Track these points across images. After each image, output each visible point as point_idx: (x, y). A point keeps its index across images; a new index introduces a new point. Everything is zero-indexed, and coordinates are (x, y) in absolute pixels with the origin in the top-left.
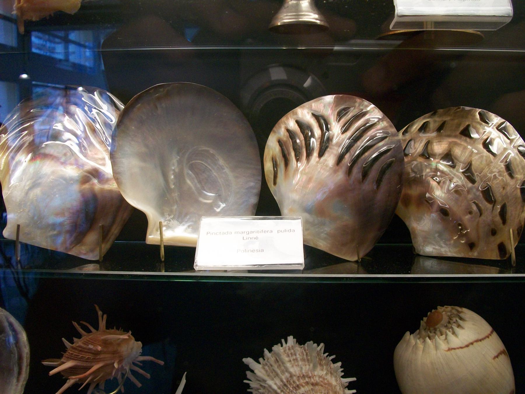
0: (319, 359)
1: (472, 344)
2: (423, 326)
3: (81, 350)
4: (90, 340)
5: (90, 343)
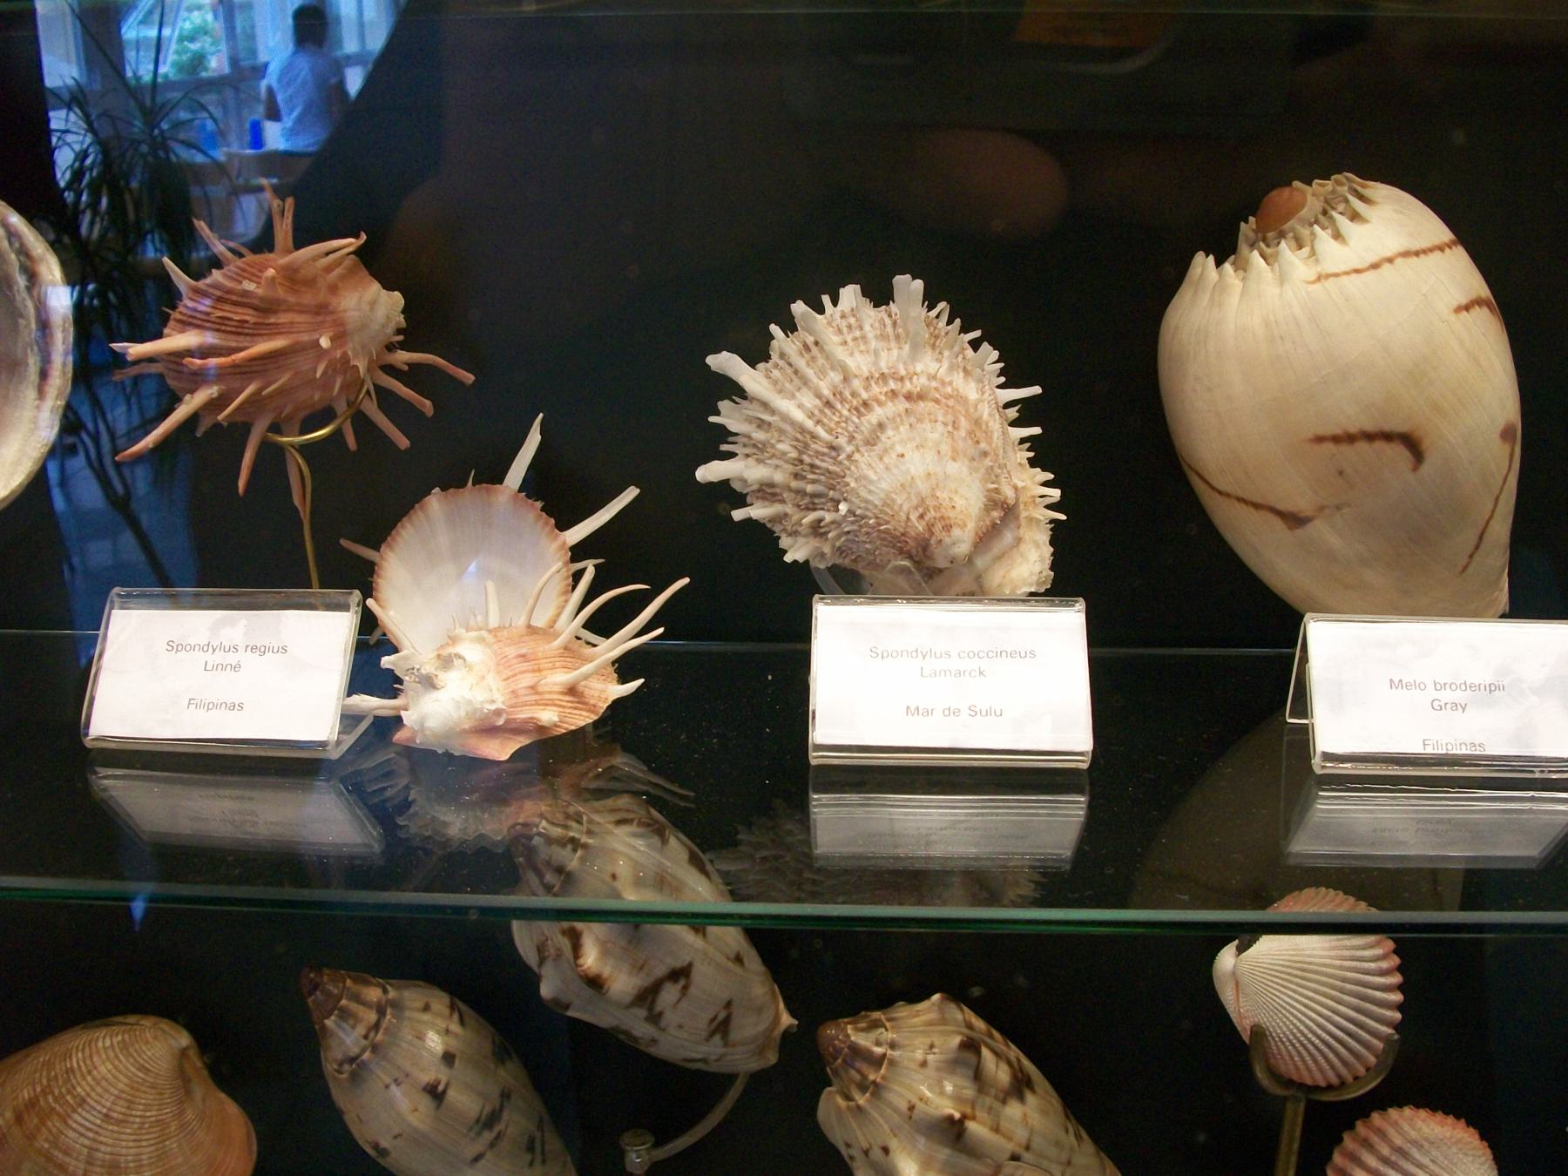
0: (931, 334)
1: (1390, 260)
2: (1246, 236)
3: (224, 297)
4: (247, 268)
5: (245, 274)
